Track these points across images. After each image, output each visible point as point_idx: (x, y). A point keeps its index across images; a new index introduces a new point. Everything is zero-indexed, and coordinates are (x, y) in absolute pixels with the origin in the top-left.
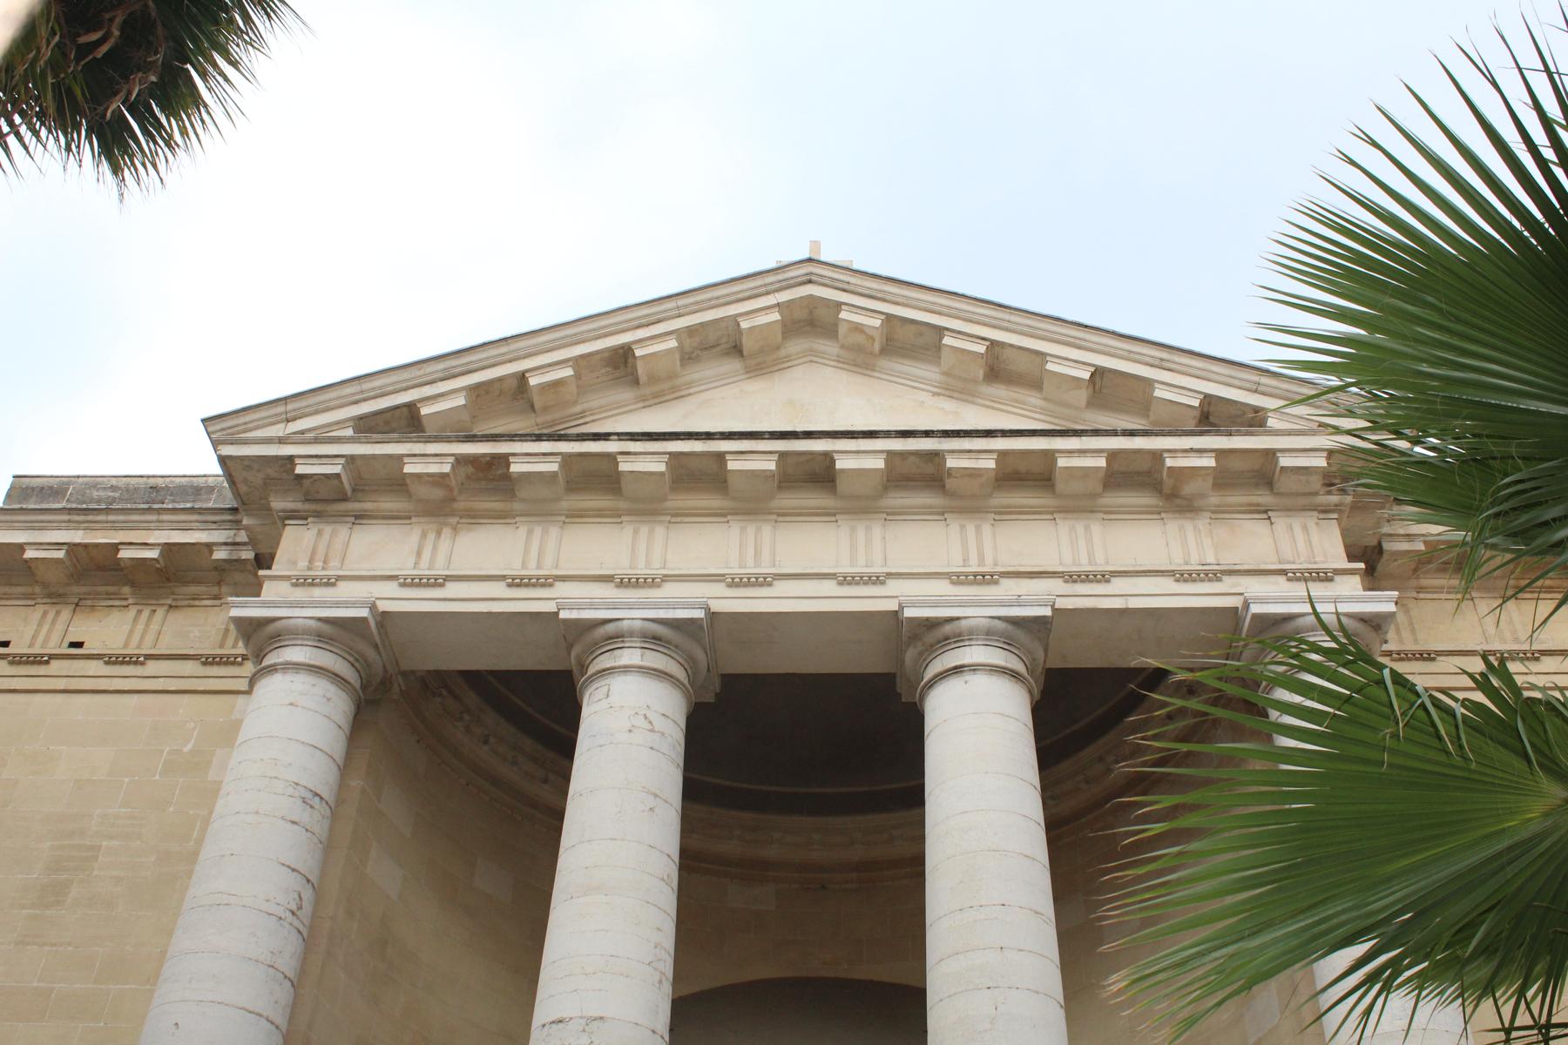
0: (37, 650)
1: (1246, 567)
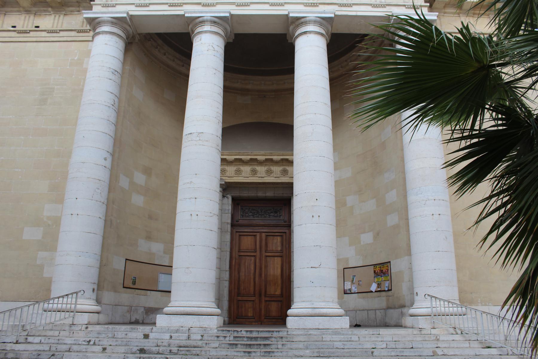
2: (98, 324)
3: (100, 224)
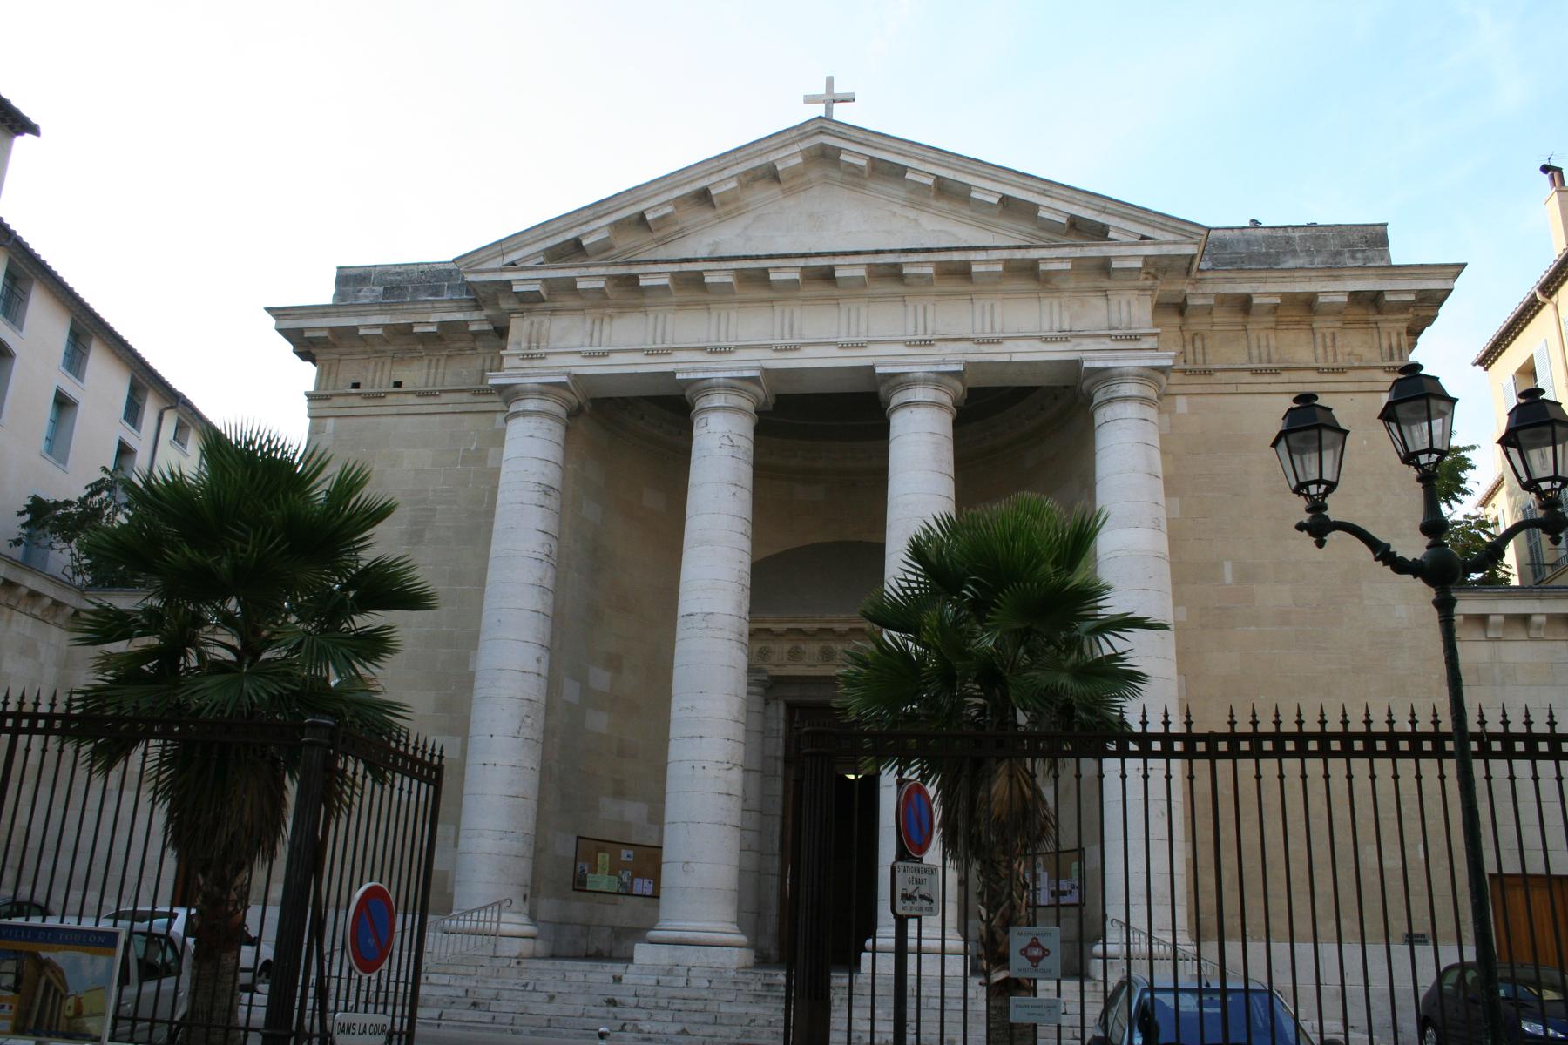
0: (376, 390)
3: (533, 779)
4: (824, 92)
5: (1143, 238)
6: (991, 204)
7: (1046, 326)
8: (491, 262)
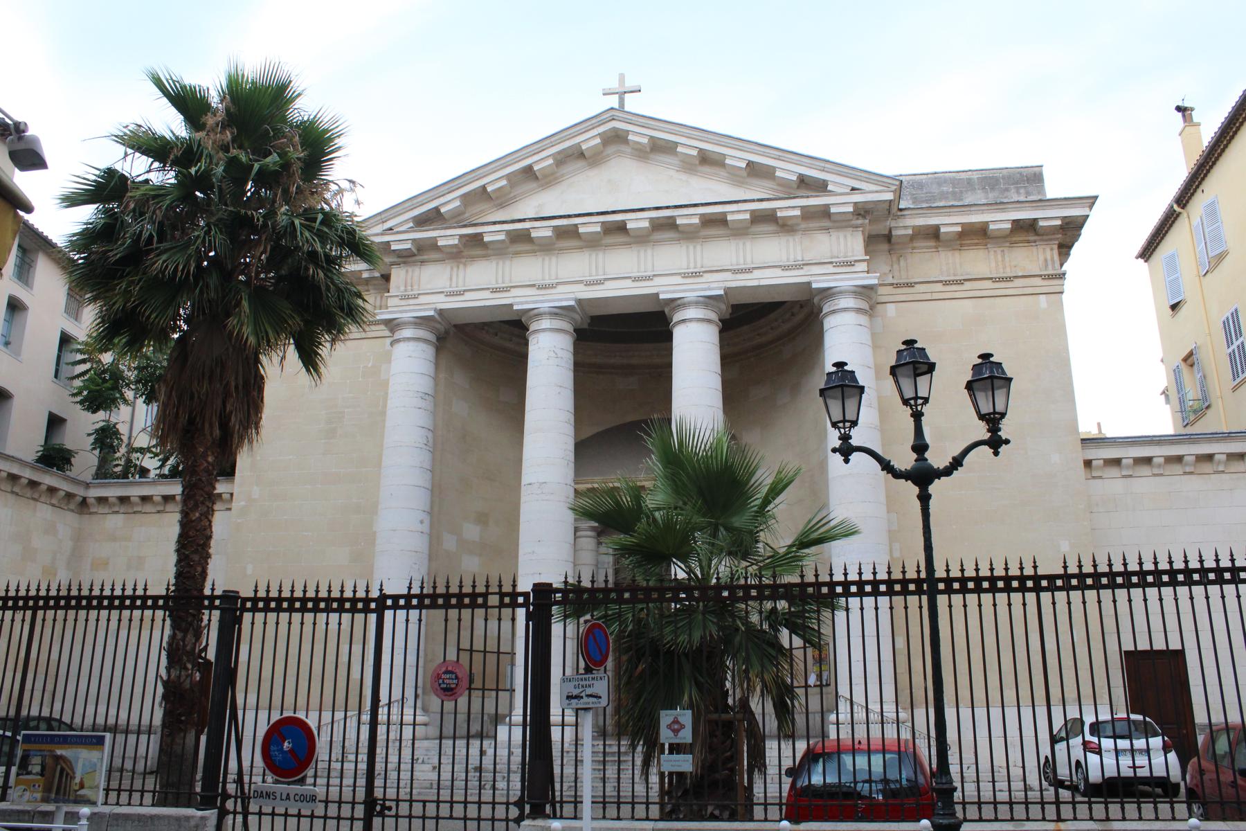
1: (814, 262)
2: (427, 739)
4: (617, 86)
5: (853, 189)
6: (740, 168)
7: (784, 258)
8: (375, 228)
